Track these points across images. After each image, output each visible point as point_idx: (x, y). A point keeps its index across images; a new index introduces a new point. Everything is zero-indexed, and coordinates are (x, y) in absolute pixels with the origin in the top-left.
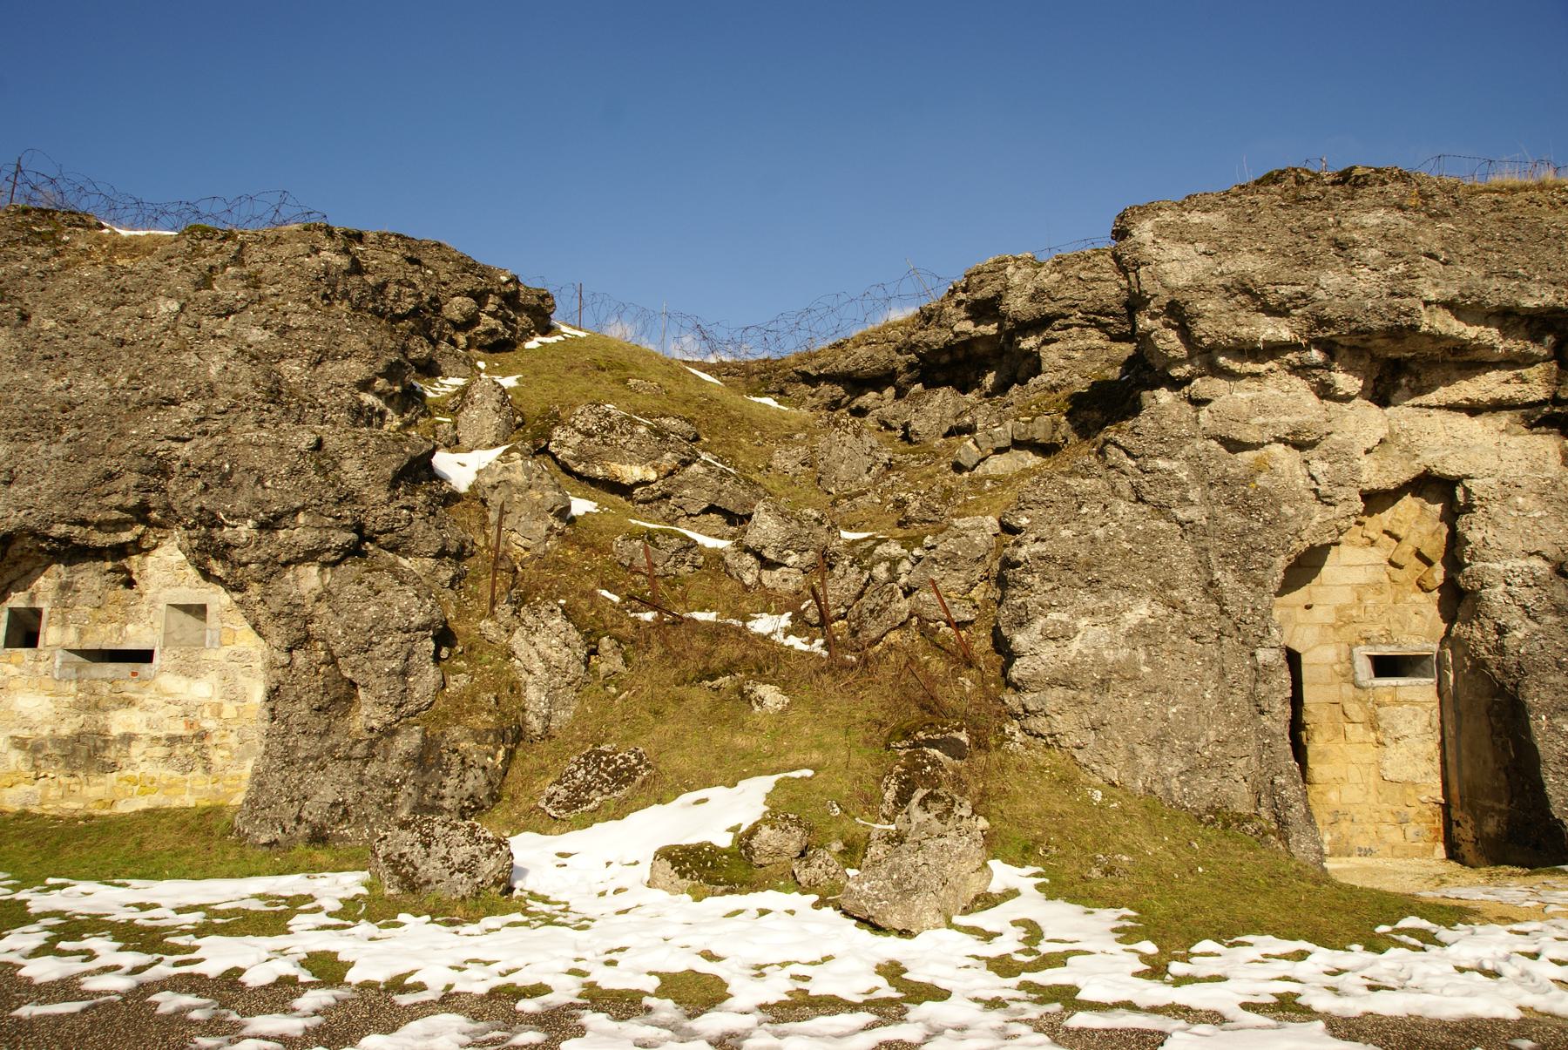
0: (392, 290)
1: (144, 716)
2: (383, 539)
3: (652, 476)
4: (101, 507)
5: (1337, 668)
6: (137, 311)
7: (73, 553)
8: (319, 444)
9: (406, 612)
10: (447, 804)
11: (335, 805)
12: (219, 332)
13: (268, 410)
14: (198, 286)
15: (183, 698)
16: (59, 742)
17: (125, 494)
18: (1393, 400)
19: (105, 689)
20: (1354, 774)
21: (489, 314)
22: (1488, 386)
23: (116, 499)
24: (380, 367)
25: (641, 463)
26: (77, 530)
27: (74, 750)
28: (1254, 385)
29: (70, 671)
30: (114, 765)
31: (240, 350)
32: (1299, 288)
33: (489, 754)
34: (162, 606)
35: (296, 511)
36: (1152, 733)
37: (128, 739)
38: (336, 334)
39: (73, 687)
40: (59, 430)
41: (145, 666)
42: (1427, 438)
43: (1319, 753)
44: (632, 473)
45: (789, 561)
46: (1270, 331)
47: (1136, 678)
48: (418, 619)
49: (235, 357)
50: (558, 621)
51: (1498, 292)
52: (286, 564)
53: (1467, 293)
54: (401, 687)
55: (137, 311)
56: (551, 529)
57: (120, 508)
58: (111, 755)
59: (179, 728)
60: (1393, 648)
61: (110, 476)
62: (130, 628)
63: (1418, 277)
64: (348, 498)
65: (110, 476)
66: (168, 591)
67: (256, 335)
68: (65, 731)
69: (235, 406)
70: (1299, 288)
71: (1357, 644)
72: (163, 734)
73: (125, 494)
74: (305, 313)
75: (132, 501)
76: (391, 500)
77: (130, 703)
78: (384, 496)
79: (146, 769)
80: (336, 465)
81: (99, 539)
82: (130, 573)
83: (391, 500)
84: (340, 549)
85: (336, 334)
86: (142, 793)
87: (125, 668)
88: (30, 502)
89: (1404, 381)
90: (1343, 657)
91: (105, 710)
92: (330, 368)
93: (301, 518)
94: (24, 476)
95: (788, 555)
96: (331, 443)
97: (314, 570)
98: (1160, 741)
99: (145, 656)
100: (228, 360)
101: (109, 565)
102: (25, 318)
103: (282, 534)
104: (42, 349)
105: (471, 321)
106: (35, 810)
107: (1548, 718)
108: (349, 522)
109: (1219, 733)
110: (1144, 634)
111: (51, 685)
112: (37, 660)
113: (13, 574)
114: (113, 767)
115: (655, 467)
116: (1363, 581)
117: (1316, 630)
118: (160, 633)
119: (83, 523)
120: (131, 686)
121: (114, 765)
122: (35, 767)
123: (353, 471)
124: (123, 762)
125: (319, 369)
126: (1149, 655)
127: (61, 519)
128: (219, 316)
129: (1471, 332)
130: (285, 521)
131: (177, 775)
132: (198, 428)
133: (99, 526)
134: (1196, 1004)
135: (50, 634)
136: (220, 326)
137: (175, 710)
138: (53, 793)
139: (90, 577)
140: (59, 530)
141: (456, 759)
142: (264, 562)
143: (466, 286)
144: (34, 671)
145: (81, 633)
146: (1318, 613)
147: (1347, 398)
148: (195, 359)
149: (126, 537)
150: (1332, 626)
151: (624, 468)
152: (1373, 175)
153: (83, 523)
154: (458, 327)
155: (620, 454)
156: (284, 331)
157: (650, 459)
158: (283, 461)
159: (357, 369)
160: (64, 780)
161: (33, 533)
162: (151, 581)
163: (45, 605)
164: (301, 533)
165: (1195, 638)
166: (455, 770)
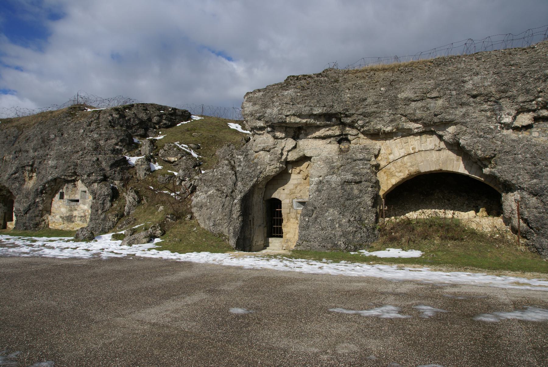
0: (132, 120)
1: (78, 212)
2: (110, 177)
3: (176, 160)
4: (68, 173)
5: (289, 204)
6: (78, 132)
7: (68, 182)
8: (98, 159)
9: (104, 192)
10: (106, 228)
11: (92, 228)
12: (90, 135)
13: (94, 152)
14: (88, 126)
15: (83, 209)
16: (66, 217)
17: (71, 170)
18: (300, 137)
19: (73, 207)
20: (292, 231)
21: (164, 120)
22: (322, 132)
23: (70, 171)
24: (119, 140)
25: (174, 157)
26: (66, 177)
27: (68, 219)
28: (262, 136)
29: (68, 204)
30: (73, 221)
31: (92, 140)
32: (261, 114)
33: (114, 219)
34: (80, 191)
35: (92, 173)
36: (208, 217)
37: (75, 216)
38: (110, 134)
39: (68, 207)
40: (64, 158)
41: (78, 203)
42: (306, 147)
43: (285, 225)
44: (173, 159)
45: (186, 179)
46: (259, 124)
47: (206, 206)
48: (106, 194)
49: (91, 141)
50: (133, 194)
51: (306, 110)
52: (92, 183)
53: (296, 112)
54: (102, 206)
55: (78, 132)
56: (145, 173)
57: (71, 173)
58: (73, 219)
59: (83, 215)
60: (302, 200)
61: (69, 167)
62: (76, 195)
63: (283, 110)
64: (103, 170)
65: (69, 167)
66: (81, 188)
67: (96, 136)
68: (67, 215)
69: (88, 152)
70: (261, 114)
71: (294, 199)
72: (80, 216)
73: (71, 170)
74: (105, 130)
75: (73, 171)
76: (111, 170)
77: (76, 210)
78: (109, 169)
79: (78, 222)
80: (101, 163)
81: (69, 179)
82: (76, 185)
83: (111, 170)
84: (100, 180)
85: (110, 134)
86: (78, 227)
87: (75, 203)
88: (58, 172)
89: (303, 132)
90: (291, 202)
91: (73, 211)
92: (109, 141)
93: (93, 174)
94: (58, 167)
95: (186, 178)
96: (100, 159)
97: (96, 184)
98: (209, 219)
99: (78, 201)
100: (89, 142)
101: (73, 183)
102: (62, 135)
103: (91, 177)
104: (64, 141)
105: (159, 122)
106: (63, 229)
107: (303, 217)
108: (102, 175)
109: (220, 218)
110: (210, 197)
111: (65, 206)
112: (64, 201)
113: (59, 186)
114: (73, 222)
115: (177, 158)
116: (296, 183)
117: (285, 195)
118: (80, 196)
119: (66, 176)
120: (76, 206)
121: (73, 221)
122: (63, 221)
123: (104, 164)
124: (75, 221)
125: (107, 142)
126: (210, 201)
127: (63, 175)
128: (90, 132)
129: (304, 121)
130: (91, 175)
131: (82, 223)
132: (81, 157)
133: (69, 176)
134: (52, 239)
135: (66, 197)
136: (90, 134)
137: (82, 211)
138: (66, 226)
139: (70, 186)
140: (63, 177)
141: (109, 219)
142: (89, 183)
143: (156, 114)
144: (63, 204)
145: (69, 196)
146: (286, 191)
147: (282, 138)
148: (84, 142)
149: (73, 178)
150: (288, 194)
151: (170, 158)
152: (303, 77)
153: (66, 176)
154: (156, 124)
155: (170, 155)
156: (100, 134)
157: (176, 156)
158: (90, 163)
159: (114, 141)
160: (67, 224)
161: (59, 178)
162: (79, 186)
163: (64, 191)
164: (93, 177)
165: (220, 197)
166: (108, 221)
